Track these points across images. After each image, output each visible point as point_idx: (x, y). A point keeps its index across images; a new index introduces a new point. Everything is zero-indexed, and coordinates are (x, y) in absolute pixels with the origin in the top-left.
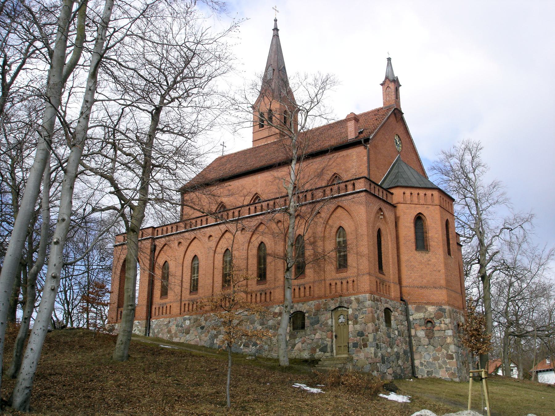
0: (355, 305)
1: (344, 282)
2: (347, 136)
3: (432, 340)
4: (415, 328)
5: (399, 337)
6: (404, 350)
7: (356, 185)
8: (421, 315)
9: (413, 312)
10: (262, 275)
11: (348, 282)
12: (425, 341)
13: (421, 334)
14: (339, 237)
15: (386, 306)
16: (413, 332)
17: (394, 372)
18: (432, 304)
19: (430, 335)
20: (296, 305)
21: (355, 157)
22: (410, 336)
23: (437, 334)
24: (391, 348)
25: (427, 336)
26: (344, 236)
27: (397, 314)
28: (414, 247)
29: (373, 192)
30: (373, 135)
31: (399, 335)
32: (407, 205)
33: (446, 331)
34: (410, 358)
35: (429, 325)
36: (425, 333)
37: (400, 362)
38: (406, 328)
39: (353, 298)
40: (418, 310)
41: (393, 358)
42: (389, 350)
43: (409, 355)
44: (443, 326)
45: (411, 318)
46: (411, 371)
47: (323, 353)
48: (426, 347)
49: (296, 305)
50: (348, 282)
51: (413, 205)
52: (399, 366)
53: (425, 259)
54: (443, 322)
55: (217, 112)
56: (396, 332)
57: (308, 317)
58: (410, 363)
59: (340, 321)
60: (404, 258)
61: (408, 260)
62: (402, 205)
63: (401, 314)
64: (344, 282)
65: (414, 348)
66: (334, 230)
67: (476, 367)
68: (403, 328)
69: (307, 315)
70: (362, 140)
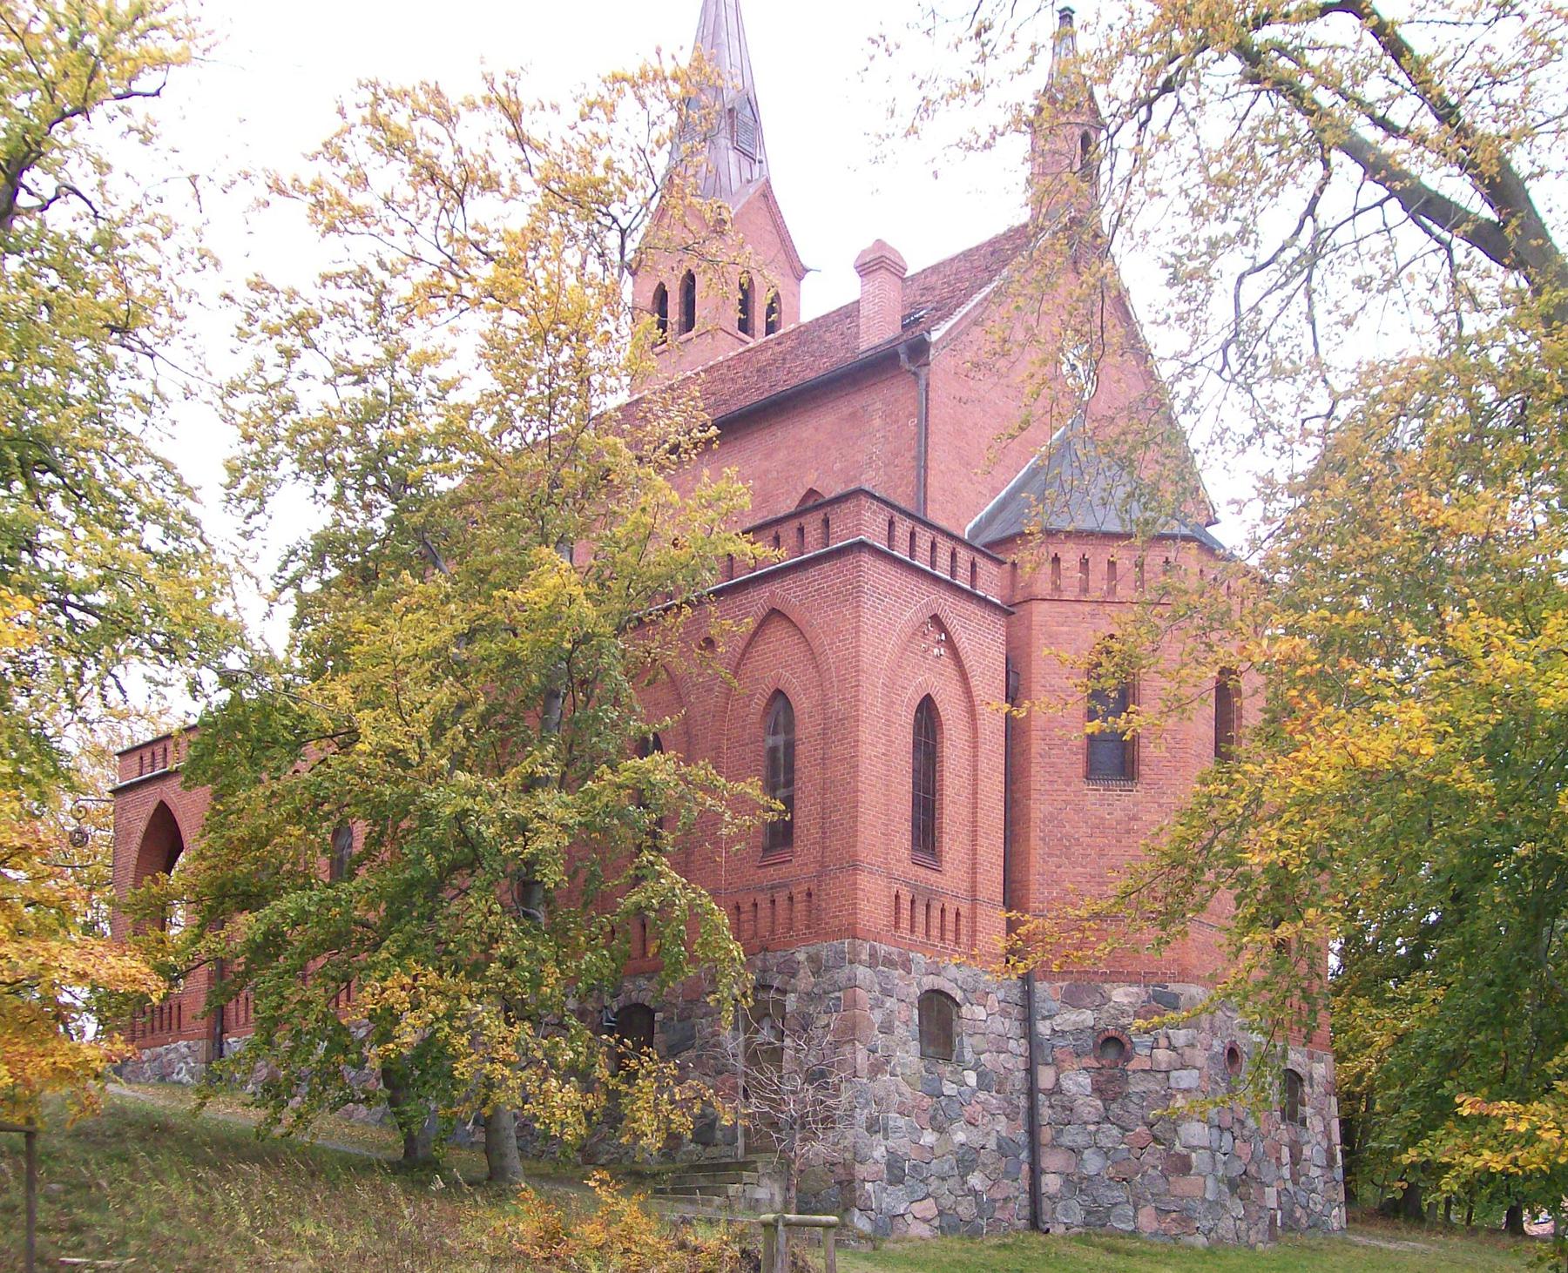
0: (805, 980)
1: (781, 898)
2: (857, 336)
3: (1115, 1108)
4: (1057, 1064)
5: (982, 1096)
6: (1000, 1140)
7: (835, 528)
8: (1087, 1017)
9: (1056, 1005)
10: (913, 902)
11: (791, 899)
12: (1090, 1107)
13: (1078, 1082)
14: (775, 733)
15: (930, 982)
16: (1046, 1077)
17: (941, 1213)
18: (1131, 979)
19: (1109, 1089)
20: (628, 985)
21: (877, 422)
22: (1032, 1091)
23: (1136, 1086)
24: (940, 1130)
25: (1098, 1090)
26: (790, 727)
27: (980, 1013)
28: (1080, 769)
29: (901, 553)
30: (945, 327)
31: (983, 1084)
32: (1066, 609)
33: (1174, 1074)
34: (1025, 1167)
35: (1112, 1052)
36: (1094, 1082)
37: (975, 1180)
38: (1021, 1063)
39: (801, 957)
40: (1072, 999)
41: (947, 1165)
42: (929, 1138)
43: (1024, 1155)
44: (1162, 1055)
45: (1043, 1028)
46: (1026, 1212)
47: (700, 1147)
48: (1092, 1128)
49: (628, 985)
50: (791, 899)
51: (1087, 608)
52: (973, 1192)
53: (1119, 814)
54: (1163, 1042)
55: (563, 267)
56: (971, 1078)
57: (663, 1024)
58: (1024, 1182)
59: (759, 1039)
60: (1039, 808)
61: (1051, 818)
62: (1045, 605)
63: (1005, 1014)
64: (781, 898)
65: (1046, 1134)
66: (759, 702)
67: (478, 1163)
68: (1012, 1062)
69: (659, 1016)
70: (901, 350)
